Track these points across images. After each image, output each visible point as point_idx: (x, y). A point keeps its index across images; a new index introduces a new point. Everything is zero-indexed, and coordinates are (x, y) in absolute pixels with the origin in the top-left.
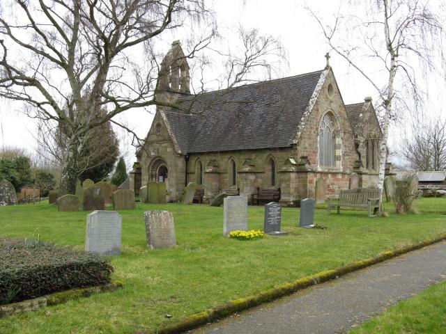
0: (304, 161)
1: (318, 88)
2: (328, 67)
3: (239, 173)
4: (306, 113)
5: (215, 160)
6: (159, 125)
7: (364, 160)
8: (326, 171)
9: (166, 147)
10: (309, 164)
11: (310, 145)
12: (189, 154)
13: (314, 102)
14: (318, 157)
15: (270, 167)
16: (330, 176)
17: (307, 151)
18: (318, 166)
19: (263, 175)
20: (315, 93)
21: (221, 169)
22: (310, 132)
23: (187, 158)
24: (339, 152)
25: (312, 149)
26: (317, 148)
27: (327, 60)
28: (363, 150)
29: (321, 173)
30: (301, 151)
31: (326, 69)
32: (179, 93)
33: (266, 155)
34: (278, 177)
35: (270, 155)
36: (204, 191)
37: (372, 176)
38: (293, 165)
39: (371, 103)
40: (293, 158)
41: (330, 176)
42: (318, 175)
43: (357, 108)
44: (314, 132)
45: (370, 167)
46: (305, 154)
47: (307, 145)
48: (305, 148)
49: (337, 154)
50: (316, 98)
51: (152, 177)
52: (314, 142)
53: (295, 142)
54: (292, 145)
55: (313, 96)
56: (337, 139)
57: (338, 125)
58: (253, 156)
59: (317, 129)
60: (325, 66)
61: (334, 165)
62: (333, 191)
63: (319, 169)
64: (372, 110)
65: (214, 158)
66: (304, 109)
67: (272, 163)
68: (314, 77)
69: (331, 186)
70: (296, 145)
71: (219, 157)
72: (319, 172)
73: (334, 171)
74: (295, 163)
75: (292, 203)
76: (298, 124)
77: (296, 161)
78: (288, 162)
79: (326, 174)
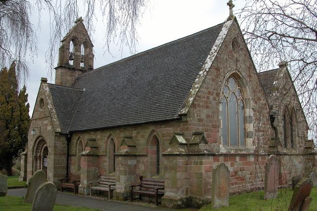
0: (197, 139)
1: (218, 42)
2: (231, 17)
3: (164, 155)
4: (201, 73)
5: (94, 140)
6: (42, 100)
7: (281, 137)
8: (233, 152)
9: (47, 125)
10: (206, 143)
11: (208, 116)
12: (72, 133)
13: (213, 58)
14: (220, 133)
15: (155, 148)
16: (238, 159)
17: (203, 125)
18: (221, 146)
19: (145, 159)
20: (214, 47)
21: (140, 150)
22: (208, 98)
23: (69, 137)
24: (251, 127)
25: (211, 122)
26: (219, 121)
27: (231, 9)
28: (280, 124)
29: (225, 155)
30: (194, 125)
31: (229, 19)
32: (81, 70)
33: (147, 132)
34: (164, 162)
35: (153, 131)
36: (80, 176)
37: (292, 157)
38: (182, 144)
39: (287, 69)
40: (182, 135)
41: (238, 159)
42: (221, 159)
43: (270, 75)
44: (214, 99)
45: (289, 146)
46: (200, 129)
47: (203, 116)
48: (200, 120)
49: (247, 114)
50: (216, 54)
51: (36, 160)
52: (213, 112)
53: (184, 111)
54: (180, 115)
55: (213, 51)
56: (247, 110)
57: (248, 93)
58: (134, 133)
59: (218, 95)
60: (228, 15)
61: (245, 144)
62: (243, 179)
63: (223, 150)
64: (288, 75)
65: (94, 137)
66: (200, 68)
67: (156, 141)
68: (213, 32)
69: (240, 173)
70: (185, 115)
71: (98, 136)
72: (222, 155)
73: (244, 152)
74: (184, 142)
75: (180, 203)
76: (190, 87)
77: (186, 140)
78: (173, 141)
79: (233, 156)
